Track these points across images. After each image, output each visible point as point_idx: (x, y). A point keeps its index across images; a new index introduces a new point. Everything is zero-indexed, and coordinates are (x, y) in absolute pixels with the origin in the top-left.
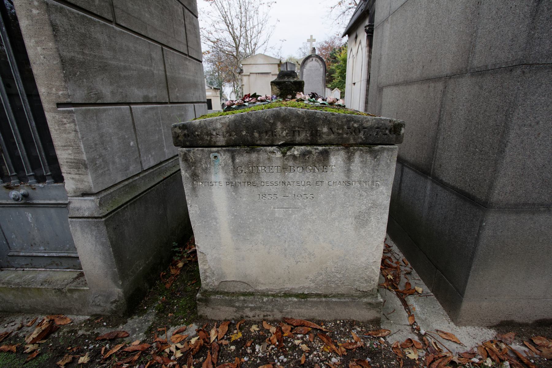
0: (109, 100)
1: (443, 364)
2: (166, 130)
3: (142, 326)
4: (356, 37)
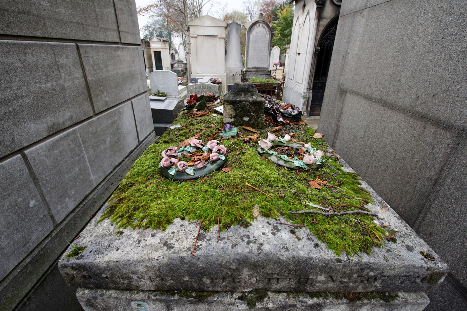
2: (91, 153)
4: (304, 6)
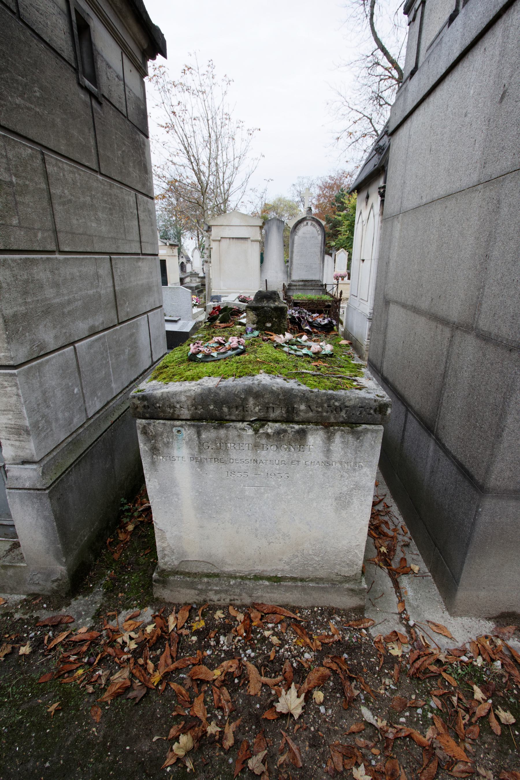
0: (52, 347)
1: (428, 662)
2: (114, 361)
3: (89, 609)
4: (368, 197)
